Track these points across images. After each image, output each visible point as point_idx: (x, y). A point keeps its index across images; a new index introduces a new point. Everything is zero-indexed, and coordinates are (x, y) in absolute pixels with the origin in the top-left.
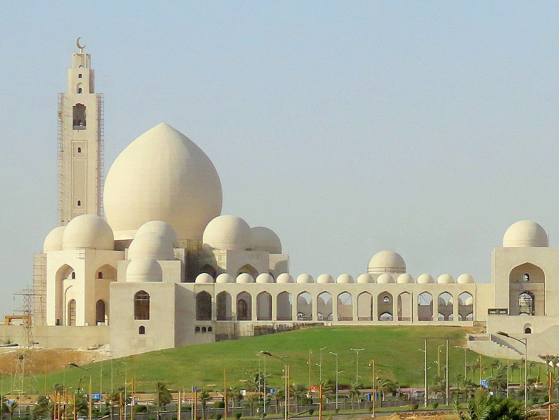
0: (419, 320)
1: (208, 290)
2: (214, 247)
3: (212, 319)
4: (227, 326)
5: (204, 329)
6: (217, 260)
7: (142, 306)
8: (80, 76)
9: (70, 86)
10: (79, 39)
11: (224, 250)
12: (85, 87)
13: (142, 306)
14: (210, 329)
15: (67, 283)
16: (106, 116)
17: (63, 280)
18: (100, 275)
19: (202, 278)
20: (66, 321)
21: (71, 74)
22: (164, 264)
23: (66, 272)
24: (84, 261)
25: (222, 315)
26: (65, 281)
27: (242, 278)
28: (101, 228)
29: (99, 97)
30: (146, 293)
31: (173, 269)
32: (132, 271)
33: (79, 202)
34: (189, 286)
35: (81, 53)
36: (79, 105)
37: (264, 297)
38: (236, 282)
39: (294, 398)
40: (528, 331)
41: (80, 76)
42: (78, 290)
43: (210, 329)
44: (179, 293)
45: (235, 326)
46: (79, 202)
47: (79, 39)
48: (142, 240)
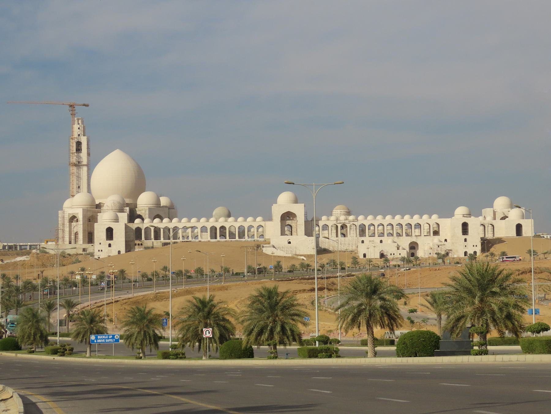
0: (122, 272)
1: (140, 226)
4: (148, 243)
7: (110, 233)
13: (110, 233)
15: (74, 224)
16: (155, 397)
19: (137, 221)
20: (73, 241)
22: (120, 215)
23: (73, 218)
27: (157, 220)
31: (124, 217)
32: (104, 220)
34: (130, 225)
37: (167, 230)
39: (380, 294)
40: (290, 243)
42: (79, 227)
43: (142, 244)
44: (126, 227)
48: (110, 201)
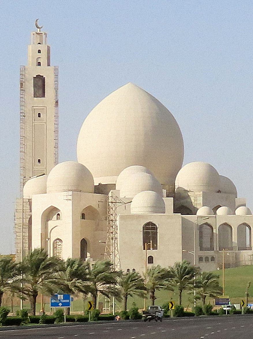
2: (188, 190)
3: (215, 249)
5: (207, 259)
6: (193, 201)
8: (39, 51)
9: (30, 59)
10: (37, 20)
11: (200, 191)
12: (43, 61)
14: (213, 259)
15: (51, 224)
17: (48, 221)
18: (83, 216)
21: (31, 49)
23: (52, 213)
24: (71, 202)
25: (225, 245)
26: (49, 222)
28: (83, 174)
29: (56, 69)
30: (155, 225)
33: (39, 161)
35: (38, 32)
36: (38, 77)
38: (235, 214)
41: (39, 51)
45: (237, 257)
46: (39, 161)
47: (37, 20)
